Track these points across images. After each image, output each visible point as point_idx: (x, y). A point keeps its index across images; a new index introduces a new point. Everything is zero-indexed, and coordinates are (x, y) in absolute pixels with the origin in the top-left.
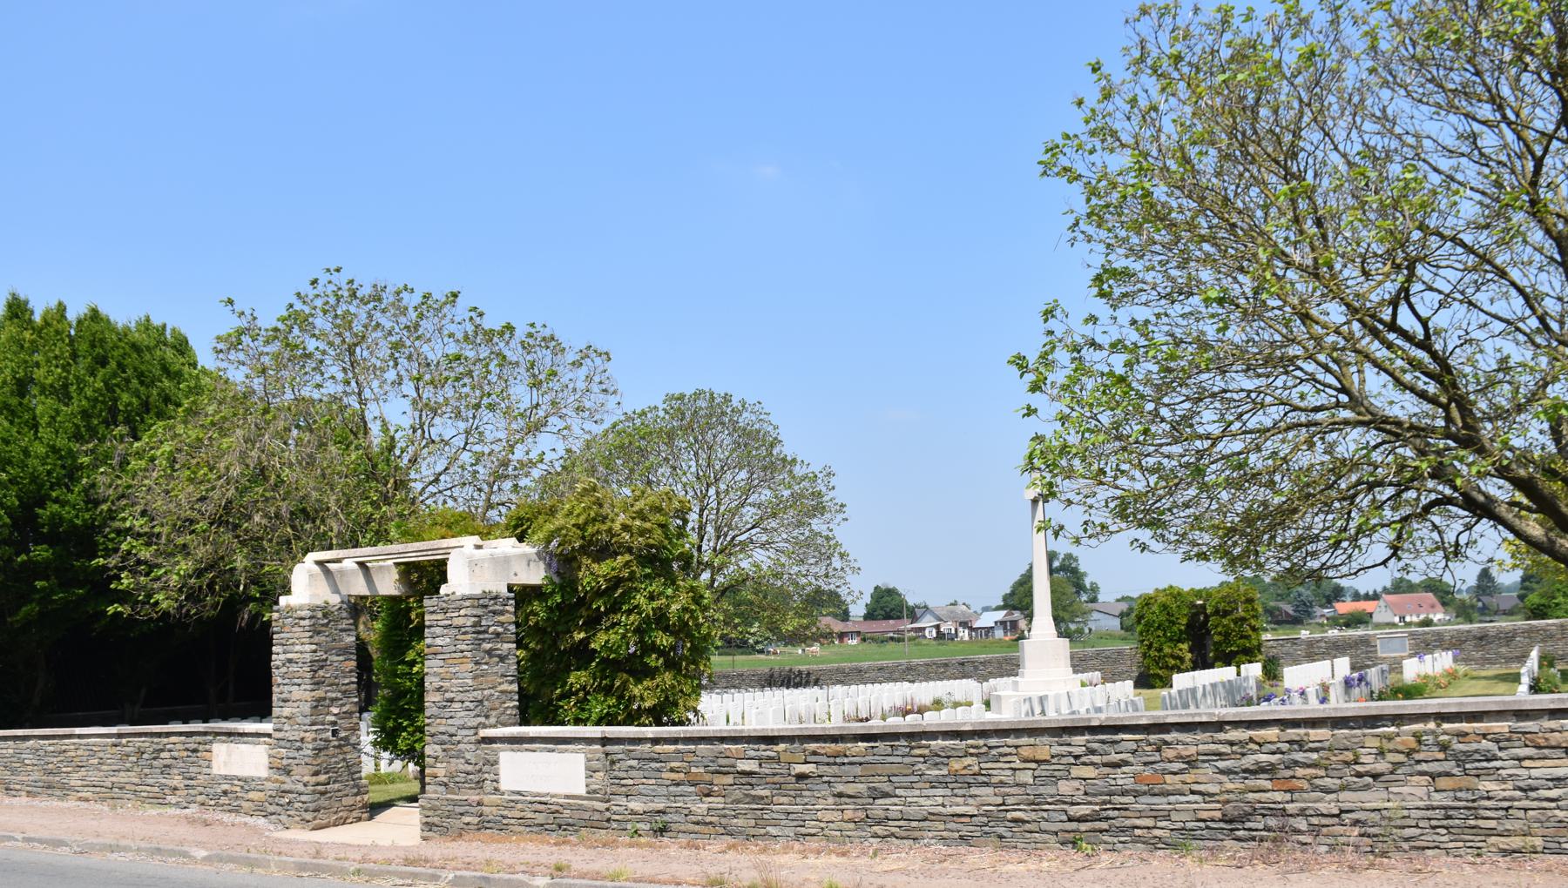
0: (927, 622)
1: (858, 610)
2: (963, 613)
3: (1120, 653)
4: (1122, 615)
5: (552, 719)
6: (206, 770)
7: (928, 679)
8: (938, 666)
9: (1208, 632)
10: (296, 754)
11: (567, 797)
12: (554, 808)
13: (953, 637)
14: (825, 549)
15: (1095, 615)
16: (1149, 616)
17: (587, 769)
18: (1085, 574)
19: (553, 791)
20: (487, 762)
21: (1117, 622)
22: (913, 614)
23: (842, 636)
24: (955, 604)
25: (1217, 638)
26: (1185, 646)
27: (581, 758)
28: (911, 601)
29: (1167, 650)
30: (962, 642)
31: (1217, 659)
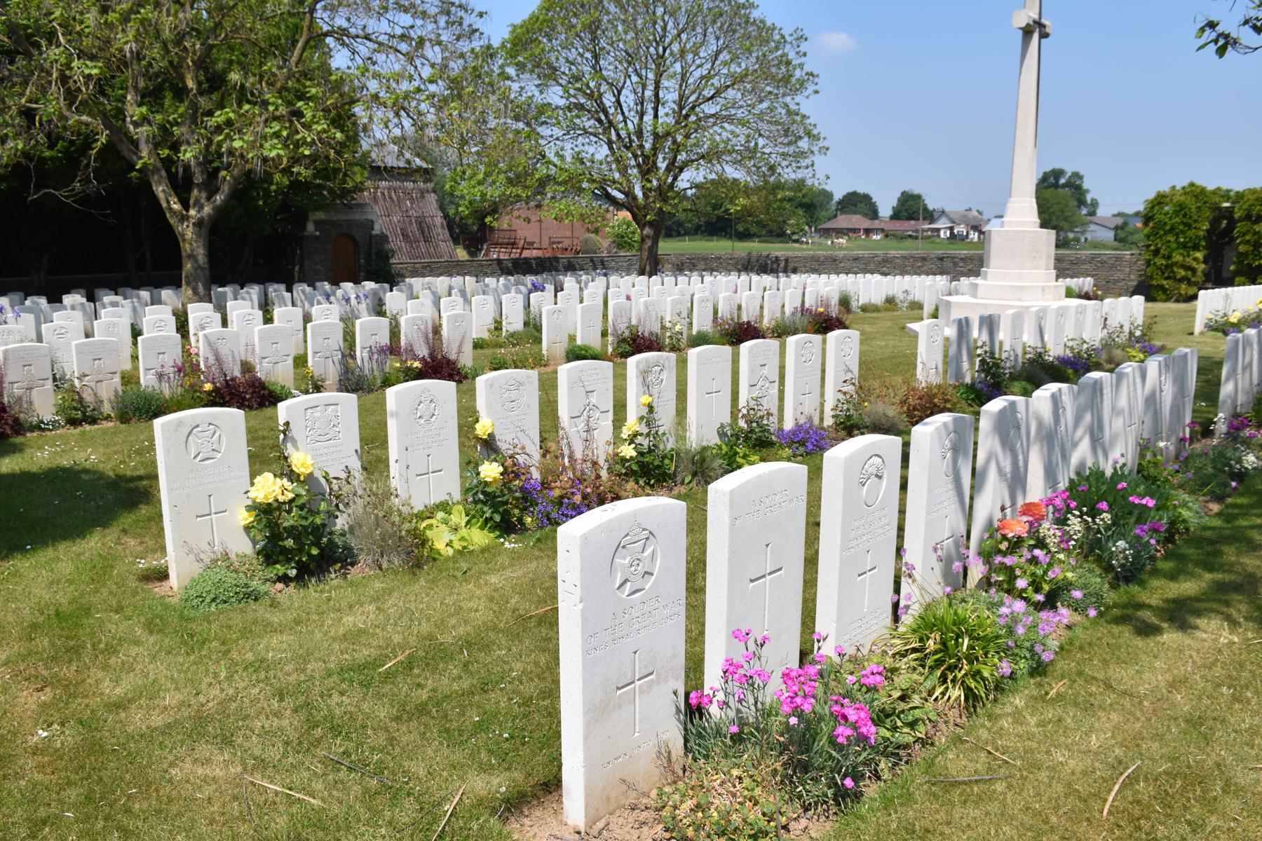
0: (942, 224)
1: (885, 211)
2: (974, 218)
3: (1118, 258)
4: (1116, 228)
7: (903, 272)
8: (916, 259)
9: (1232, 239)
13: (964, 238)
14: (794, 130)
15: (1092, 227)
16: (1159, 217)
18: (1087, 191)
21: (1111, 234)
22: (930, 216)
23: (868, 232)
24: (970, 209)
25: (1242, 248)
26: (1200, 255)
28: (931, 205)
29: (1177, 257)
30: (972, 242)
31: (1238, 273)
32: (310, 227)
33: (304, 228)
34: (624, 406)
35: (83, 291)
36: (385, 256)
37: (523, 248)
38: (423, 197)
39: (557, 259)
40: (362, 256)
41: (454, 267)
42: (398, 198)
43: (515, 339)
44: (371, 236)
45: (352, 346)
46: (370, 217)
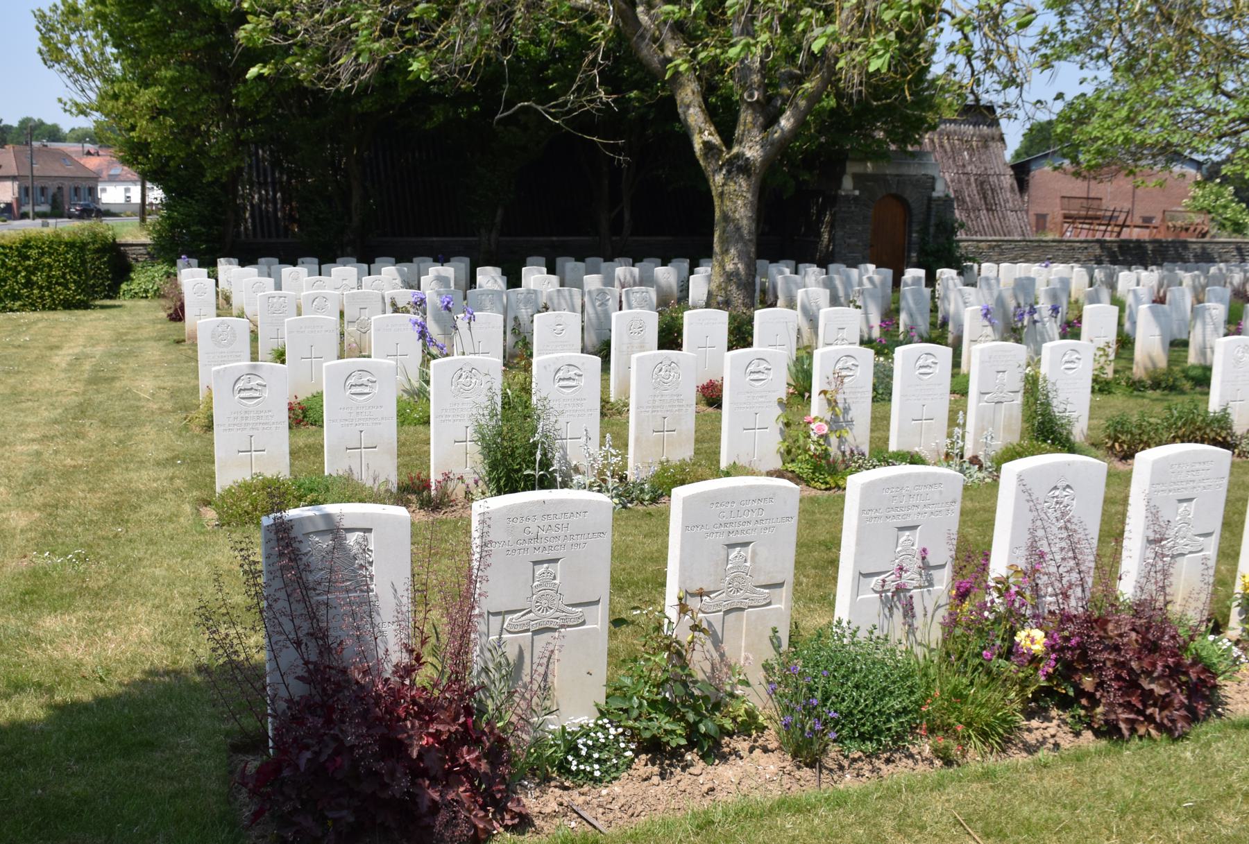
32: (847, 183)
33: (839, 184)
34: (1119, 537)
35: (543, 260)
36: (948, 229)
37: (1123, 226)
38: (986, 147)
39: (1185, 244)
40: (916, 228)
41: (1034, 248)
42: (953, 146)
43: (1162, 383)
44: (930, 199)
45: (808, 375)
46: (930, 172)
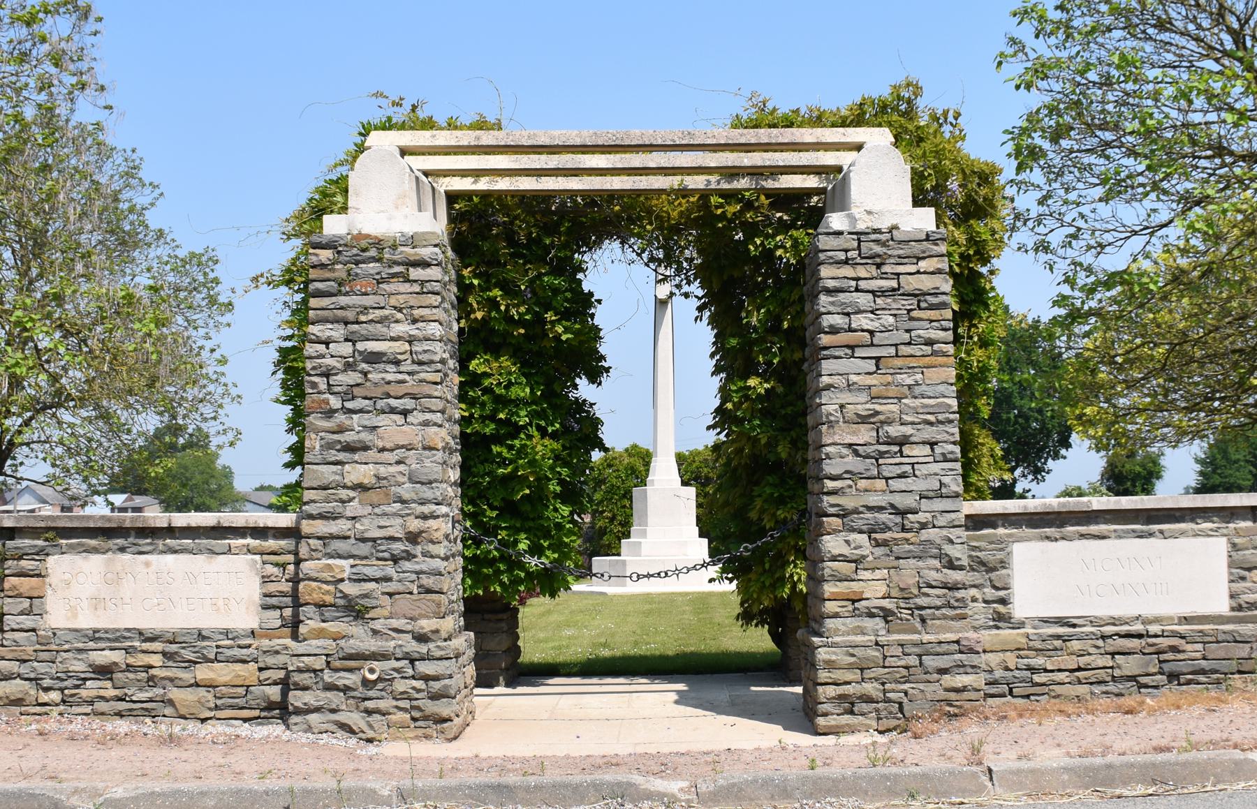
5: (491, 686)
6: (28, 622)
10: (390, 570)
11: (1186, 620)
12: (1164, 642)
17: (1231, 565)
19: (1148, 611)
20: (981, 565)
27: (1220, 546)
